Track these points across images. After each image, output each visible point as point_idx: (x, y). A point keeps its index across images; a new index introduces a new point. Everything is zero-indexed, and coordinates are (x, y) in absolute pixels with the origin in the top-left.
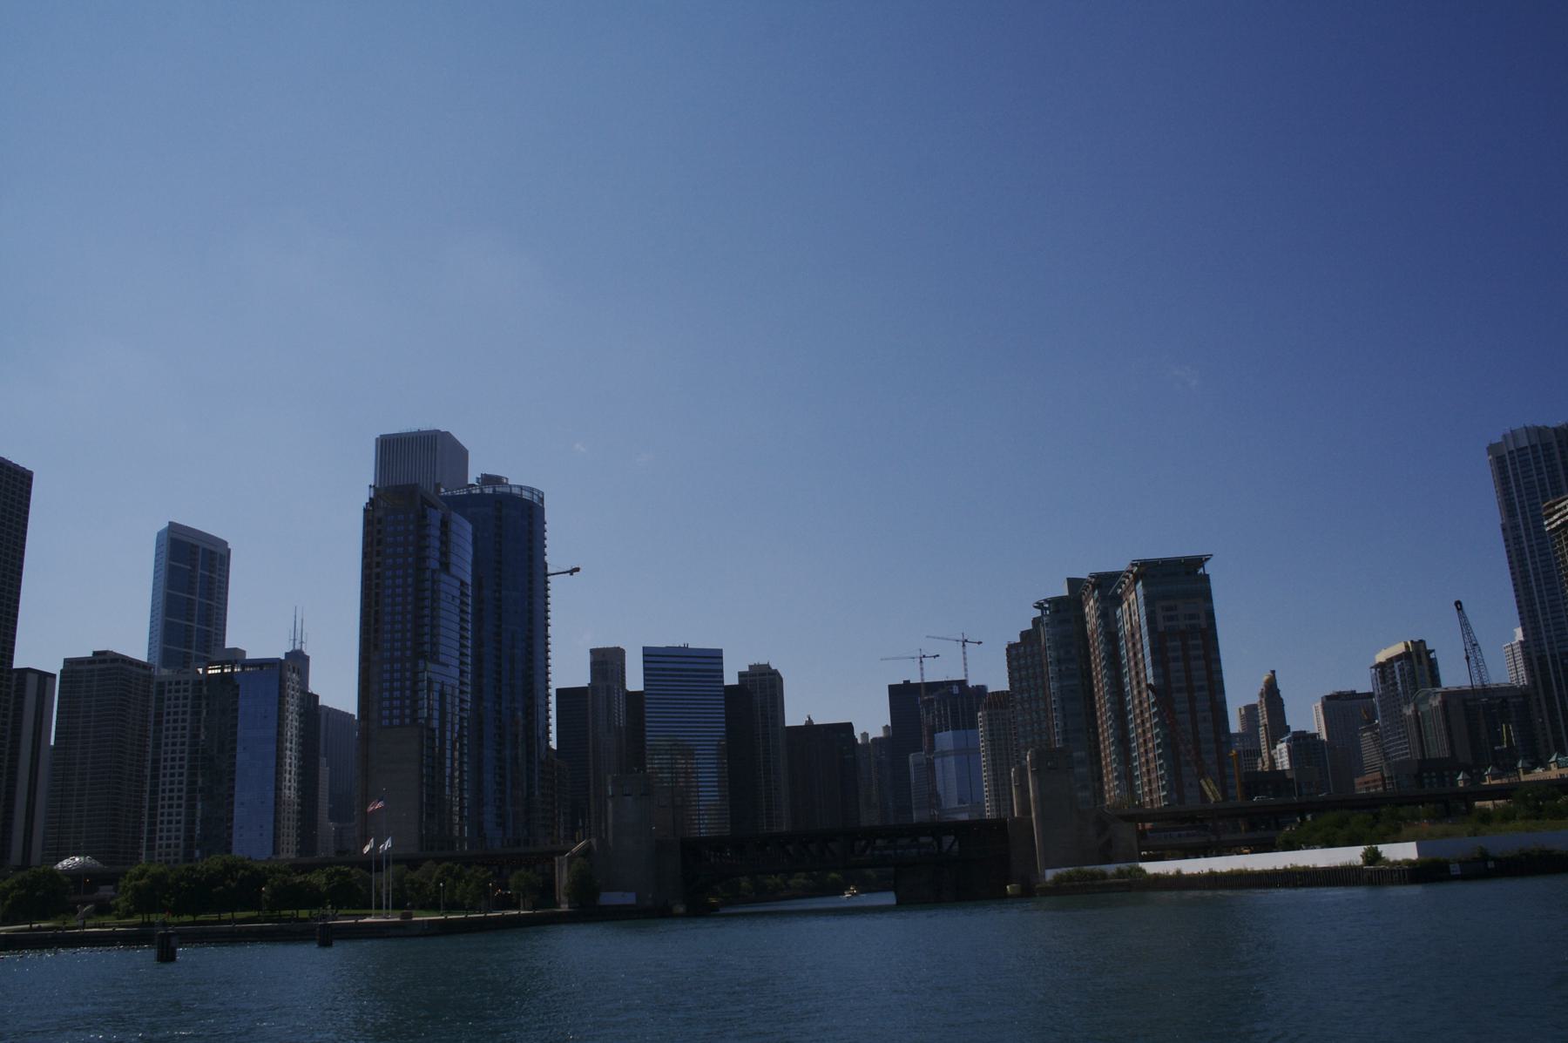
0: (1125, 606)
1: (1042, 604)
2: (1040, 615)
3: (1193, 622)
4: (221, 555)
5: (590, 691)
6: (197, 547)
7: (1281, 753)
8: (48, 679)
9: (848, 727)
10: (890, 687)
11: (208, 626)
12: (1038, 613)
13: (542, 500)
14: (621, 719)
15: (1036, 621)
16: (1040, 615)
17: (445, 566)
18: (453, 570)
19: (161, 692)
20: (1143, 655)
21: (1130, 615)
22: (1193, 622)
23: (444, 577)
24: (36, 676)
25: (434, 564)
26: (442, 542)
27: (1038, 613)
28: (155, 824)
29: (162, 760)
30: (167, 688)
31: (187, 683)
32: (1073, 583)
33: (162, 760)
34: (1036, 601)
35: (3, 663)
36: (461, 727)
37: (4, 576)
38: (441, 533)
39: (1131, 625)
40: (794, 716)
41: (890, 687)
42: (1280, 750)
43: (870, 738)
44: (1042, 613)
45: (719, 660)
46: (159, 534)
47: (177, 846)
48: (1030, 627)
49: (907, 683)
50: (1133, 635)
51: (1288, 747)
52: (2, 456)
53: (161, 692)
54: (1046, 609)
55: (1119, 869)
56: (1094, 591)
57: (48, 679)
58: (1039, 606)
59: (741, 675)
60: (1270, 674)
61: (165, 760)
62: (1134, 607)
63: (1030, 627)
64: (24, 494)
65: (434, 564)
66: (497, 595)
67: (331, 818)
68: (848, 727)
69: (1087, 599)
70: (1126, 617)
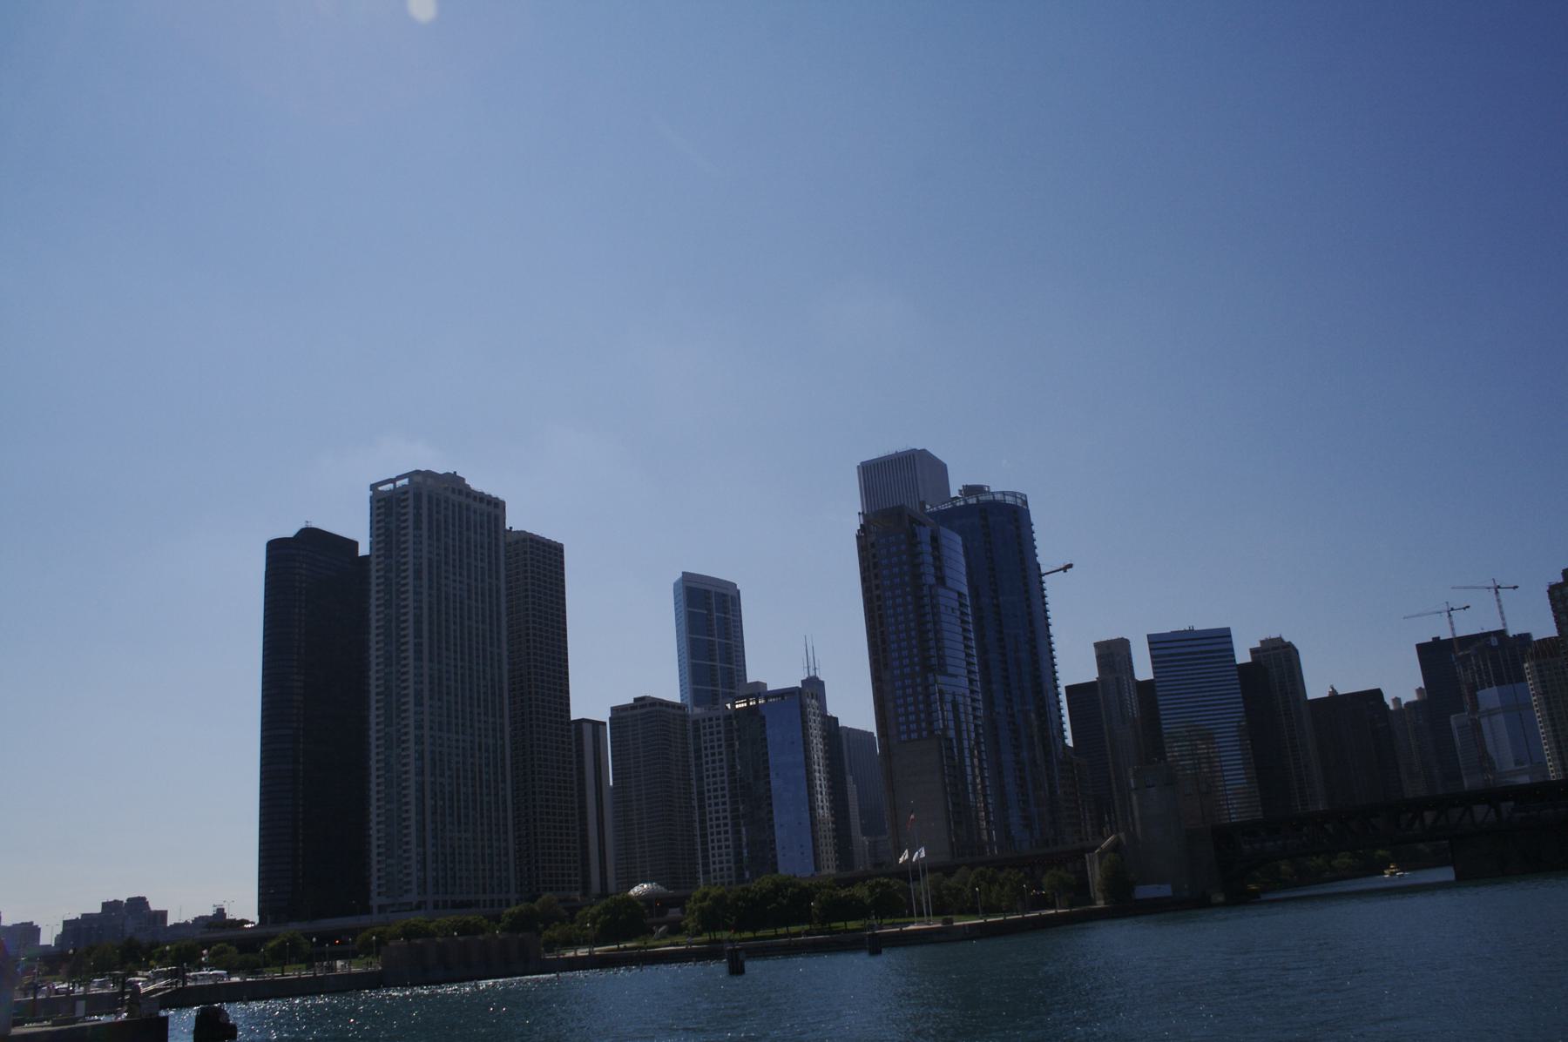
9: (1376, 694)
17: (941, 580)
19: (697, 730)
23: (941, 591)
26: (934, 548)
30: (702, 724)
36: (977, 735)
40: (1315, 689)
49: (1436, 640)
53: (697, 730)
66: (995, 601)
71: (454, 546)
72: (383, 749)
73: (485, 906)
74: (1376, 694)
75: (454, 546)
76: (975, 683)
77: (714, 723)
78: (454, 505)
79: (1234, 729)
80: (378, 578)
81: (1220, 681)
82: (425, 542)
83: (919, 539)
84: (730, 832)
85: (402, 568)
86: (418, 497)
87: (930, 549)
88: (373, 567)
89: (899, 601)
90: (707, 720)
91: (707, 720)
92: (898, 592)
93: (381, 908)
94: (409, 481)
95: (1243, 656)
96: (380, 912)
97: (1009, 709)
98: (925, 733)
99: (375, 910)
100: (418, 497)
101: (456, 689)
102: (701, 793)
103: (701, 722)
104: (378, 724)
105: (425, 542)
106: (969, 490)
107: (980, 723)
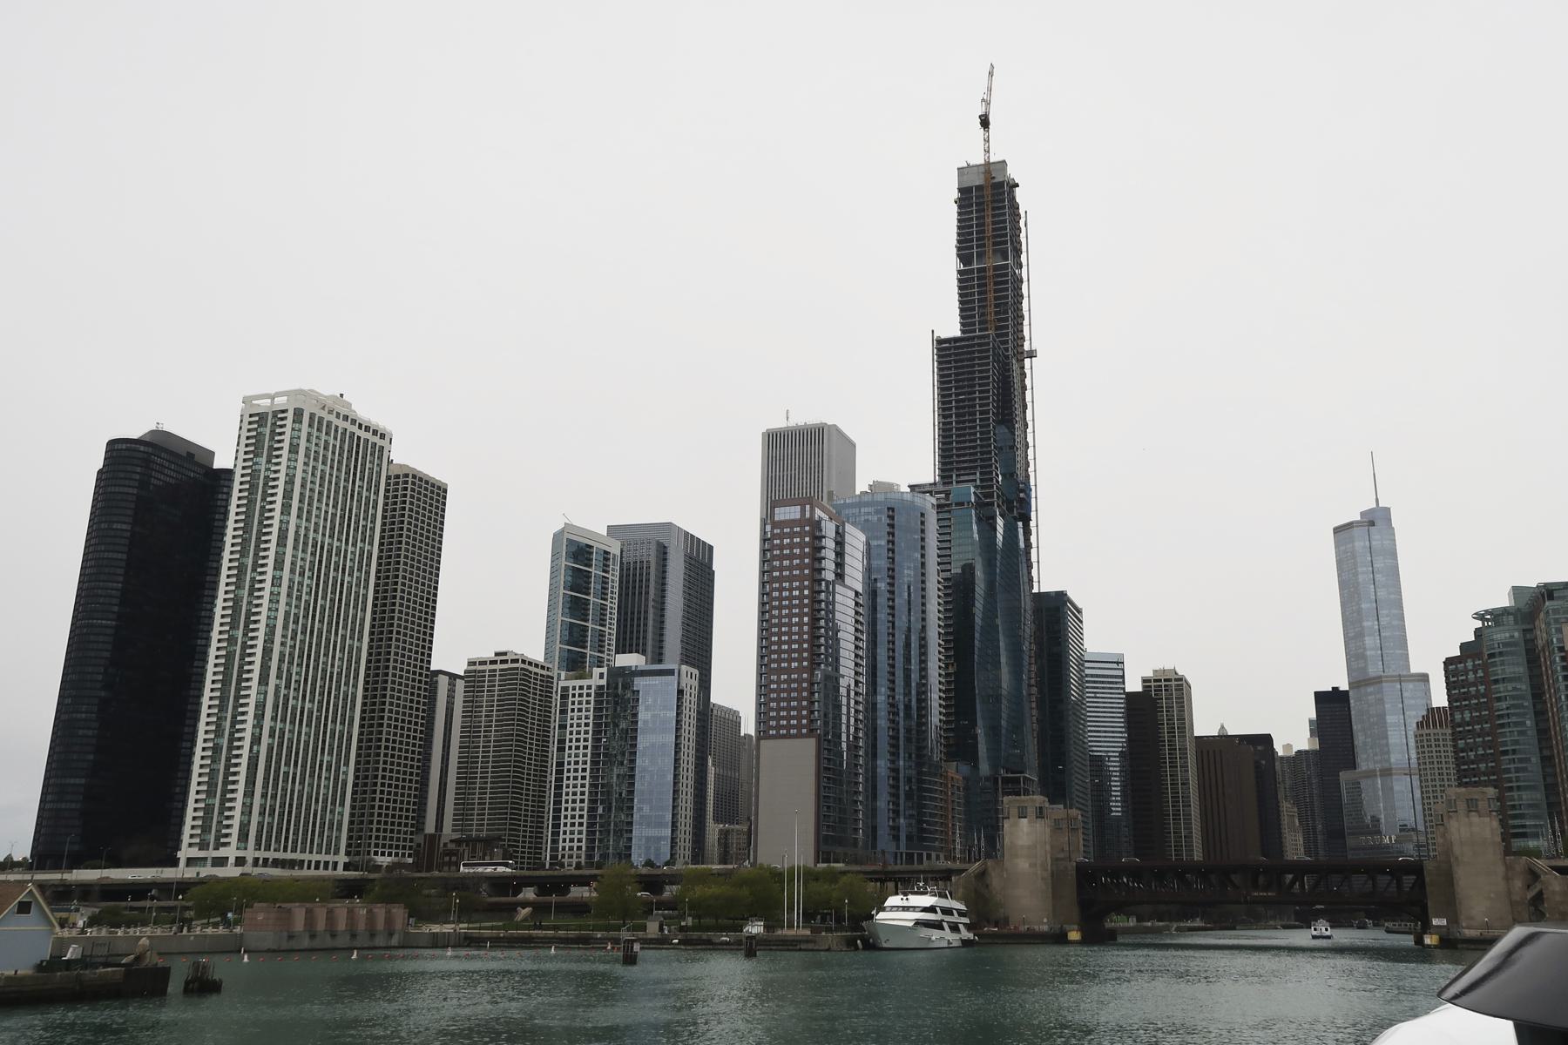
2: (1481, 626)
4: (614, 555)
6: (591, 547)
9: (1267, 740)
10: (1315, 693)
11: (600, 651)
12: (1479, 624)
15: (1477, 632)
16: (1481, 626)
17: (840, 576)
18: (848, 581)
19: (564, 697)
23: (838, 588)
25: (829, 575)
26: (837, 543)
27: (1479, 624)
28: (559, 818)
29: (570, 696)
30: (571, 692)
31: (589, 687)
33: (570, 696)
36: (857, 729)
38: (836, 544)
40: (1204, 724)
41: (1315, 693)
43: (1295, 749)
44: (1483, 624)
47: (579, 848)
48: (1472, 638)
49: (1335, 689)
53: (564, 697)
54: (1488, 620)
58: (1480, 616)
59: (1145, 681)
61: (571, 741)
63: (1472, 638)
64: (436, 551)
65: (829, 575)
66: (891, 603)
67: (717, 820)
71: (331, 475)
72: (209, 762)
73: (309, 868)
74: (1267, 740)
75: (331, 475)
76: (860, 685)
77: (585, 691)
78: (336, 431)
79: (1121, 715)
80: (205, 741)
81: (1113, 693)
82: (283, 599)
83: (823, 533)
84: (585, 816)
85: (278, 430)
86: (298, 414)
87: (834, 544)
88: (237, 479)
89: (796, 593)
90: (577, 688)
91: (577, 688)
92: (796, 584)
93: (191, 862)
94: (288, 400)
95: (1134, 685)
96: (188, 865)
97: (891, 698)
98: (804, 731)
99: (182, 863)
100: (298, 414)
101: (334, 446)
102: (560, 764)
103: (571, 689)
104: (194, 818)
105: (283, 599)
106: (876, 486)
107: (861, 700)
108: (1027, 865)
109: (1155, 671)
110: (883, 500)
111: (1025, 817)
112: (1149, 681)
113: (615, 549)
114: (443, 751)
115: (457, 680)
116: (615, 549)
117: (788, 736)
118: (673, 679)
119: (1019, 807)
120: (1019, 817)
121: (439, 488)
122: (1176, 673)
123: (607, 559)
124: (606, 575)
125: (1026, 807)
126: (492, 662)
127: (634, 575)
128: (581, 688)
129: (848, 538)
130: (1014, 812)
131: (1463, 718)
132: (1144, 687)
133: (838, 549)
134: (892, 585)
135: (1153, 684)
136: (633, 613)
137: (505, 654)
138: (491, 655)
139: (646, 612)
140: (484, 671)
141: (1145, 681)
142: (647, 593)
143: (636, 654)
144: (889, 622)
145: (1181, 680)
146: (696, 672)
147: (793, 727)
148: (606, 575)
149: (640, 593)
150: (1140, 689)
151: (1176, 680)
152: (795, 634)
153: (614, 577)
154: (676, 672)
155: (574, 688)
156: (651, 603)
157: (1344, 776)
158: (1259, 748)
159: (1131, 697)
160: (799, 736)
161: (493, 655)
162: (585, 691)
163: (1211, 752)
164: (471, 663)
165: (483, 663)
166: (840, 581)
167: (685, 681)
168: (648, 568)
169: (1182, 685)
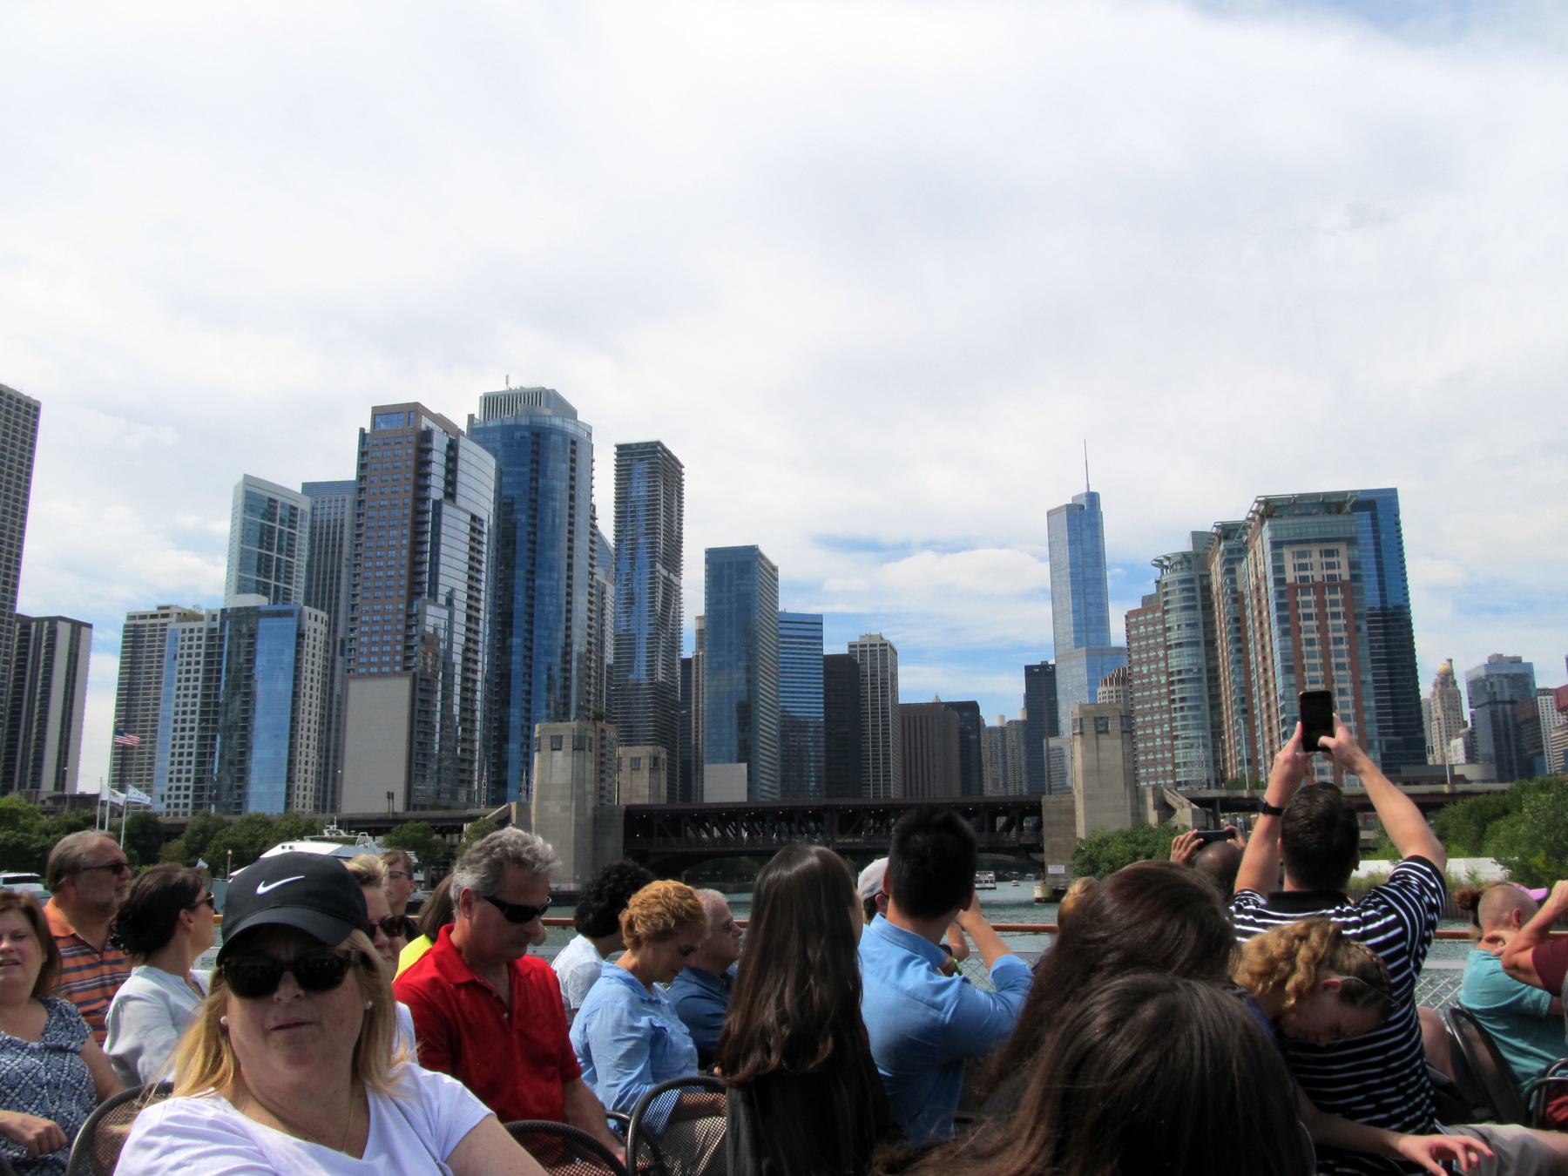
0: (1251, 555)
1: (1161, 561)
3: (1331, 572)
4: (302, 511)
5: (694, 663)
6: (275, 501)
7: (1455, 751)
8: (84, 629)
9: (971, 708)
13: (590, 435)
14: (811, 707)
17: (451, 495)
18: (461, 501)
20: (1269, 613)
21: (1256, 565)
22: (1331, 572)
24: (68, 626)
31: (200, 630)
32: (1197, 536)
34: (1154, 557)
35: (4, 606)
37: (5, 512)
39: (1257, 577)
42: (1455, 747)
43: (1007, 720)
45: (818, 627)
46: (236, 487)
50: (1258, 589)
51: (1465, 743)
52: (4, 383)
55: (23, 1121)
56: (1220, 543)
57: (84, 629)
60: (1445, 662)
62: (1260, 555)
65: (436, 493)
68: (971, 708)
69: (1213, 555)
70: (1252, 568)
77: (196, 635)
108: (558, 809)
109: (862, 637)
110: (528, 423)
111: (560, 749)
112: (855, 646)
113: (305, 505)
114: (65, 704)
115: (744, 766)
116: (305, 505)
117: (382, 675)
118: (291, 623)
119: (552, 737)
120: (553, 749)
121: (28, 405)
122: (882, 639)
123: (294, 515)
124: (293, 531)
125: (561, 737)
126: (154, 616)
127: (335, 533)
128: (192, 631)
129: (461, 453)
130: (546, 743)
131: (1141, 671)
132: (850, 652)
133: (451, 465)
134: (534, 517)
135: (868, 649)
136: (332, 572)
137: (168, 608)
138: (154, 610)
139: (339, 571)
140: (144, 626)
141: (851, 646)
142: (340, 552)
143: (255, 595)
144: (529, 558)
145: (886, 645)
146: (323, 615)
147: (386, 664)
148: (293, 531)
149: (333, 552)
150: (847, 652)
151: (881, 645)
152: (393, 559)
153: (303, 536)
154: (296, 613)
155: (184, 631)
156: (344, 562)
157: (1053, 742)
158: (966, 714)
159: (832, 661)
160: (393, 674)
161: (155, 609)
162: (196, 635)
163: (918, 719)
164: (131, 617)
165: (143, 617)
166: (450, 501)
167: (309, 624)
168: (342, 526)
169: (886, 650)
